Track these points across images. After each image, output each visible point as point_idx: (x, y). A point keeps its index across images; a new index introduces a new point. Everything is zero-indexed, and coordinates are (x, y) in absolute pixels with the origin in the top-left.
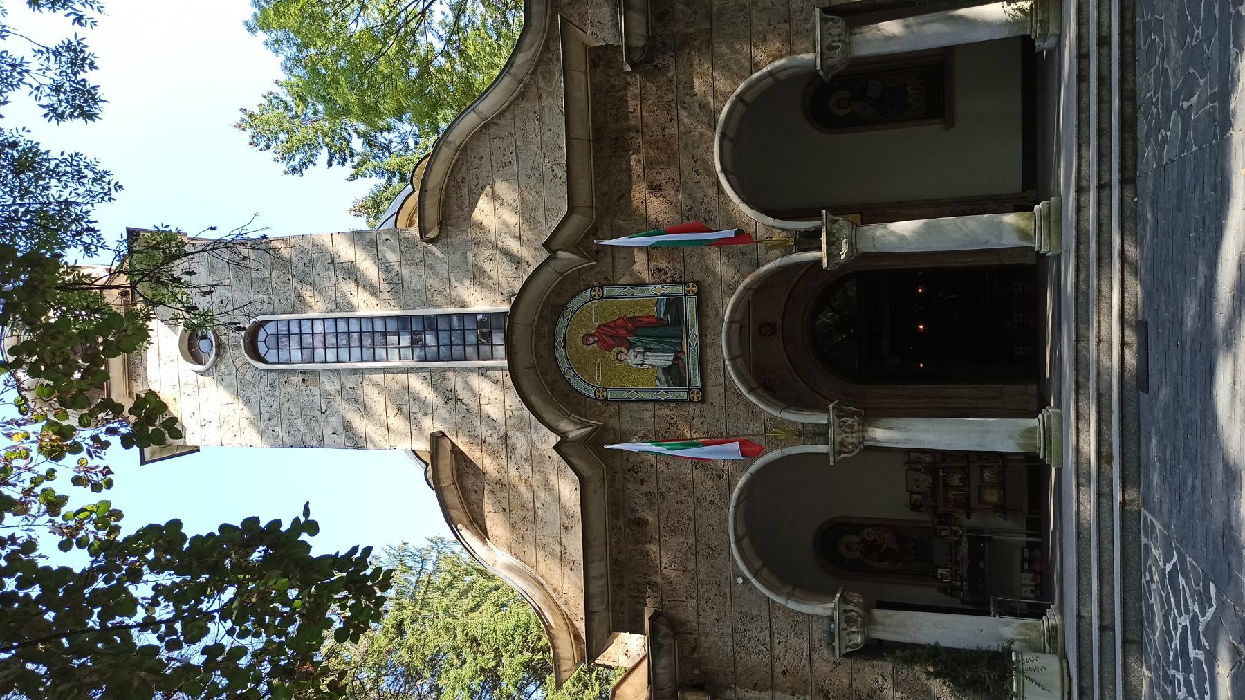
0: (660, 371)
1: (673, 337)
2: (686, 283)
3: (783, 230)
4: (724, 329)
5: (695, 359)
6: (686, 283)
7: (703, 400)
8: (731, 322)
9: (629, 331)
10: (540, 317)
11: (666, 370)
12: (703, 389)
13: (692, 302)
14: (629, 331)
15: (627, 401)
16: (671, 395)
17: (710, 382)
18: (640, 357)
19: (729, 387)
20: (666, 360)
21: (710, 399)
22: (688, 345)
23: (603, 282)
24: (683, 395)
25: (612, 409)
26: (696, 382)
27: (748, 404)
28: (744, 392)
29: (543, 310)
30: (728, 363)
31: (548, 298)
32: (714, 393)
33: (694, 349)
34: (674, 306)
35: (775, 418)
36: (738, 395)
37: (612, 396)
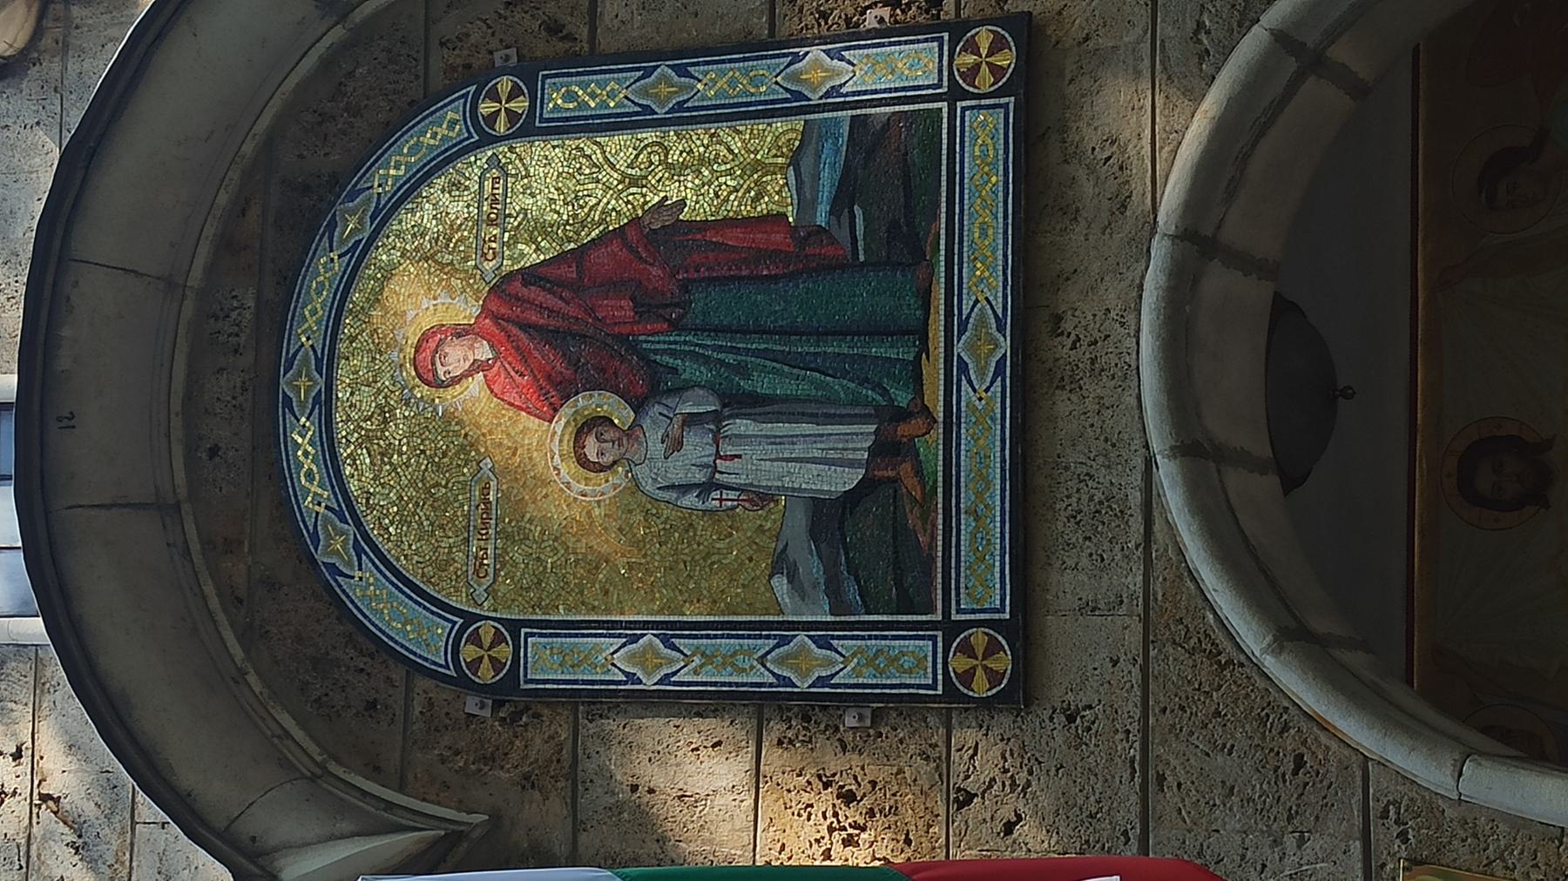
0: (799, 520)
1: (880, 332)
2: (959, 30)
3: (623, 672)
4: (1154, 280)
5: (984, 448)
6: (959, 30)
7: (1019, 694)
8: (1198, 241)
9: (647, 306)
10: (227, 245)
11: (828, 517)
12: (1022, 627)
13: (984, 137)
14: (647, 306)
15: (1146, 620)
16: (846, 664)
17: (1068, 583)
18: (697, 447)
19: (1169, 616)
20: (816, 460)
21: (1057, 692)
22: (955, 371)
23: (542, 47)
24: (912, 660)
25: (538, 741)
26: (985, 587)
27: (1276, 713)
28: (1251, 635)
29: (240, 209)
30: (1168, 474)
31: (270, 143)
32: (1090, 651)
33: (985, 400)
34: (889, 166)
35: (1429, 806)
36: (1221, 656)
37: (545, 663)
